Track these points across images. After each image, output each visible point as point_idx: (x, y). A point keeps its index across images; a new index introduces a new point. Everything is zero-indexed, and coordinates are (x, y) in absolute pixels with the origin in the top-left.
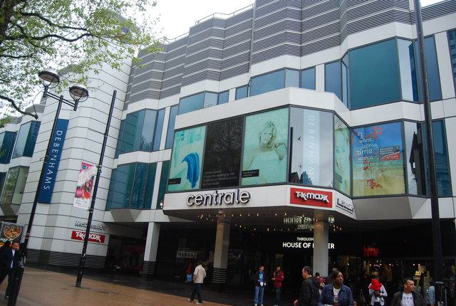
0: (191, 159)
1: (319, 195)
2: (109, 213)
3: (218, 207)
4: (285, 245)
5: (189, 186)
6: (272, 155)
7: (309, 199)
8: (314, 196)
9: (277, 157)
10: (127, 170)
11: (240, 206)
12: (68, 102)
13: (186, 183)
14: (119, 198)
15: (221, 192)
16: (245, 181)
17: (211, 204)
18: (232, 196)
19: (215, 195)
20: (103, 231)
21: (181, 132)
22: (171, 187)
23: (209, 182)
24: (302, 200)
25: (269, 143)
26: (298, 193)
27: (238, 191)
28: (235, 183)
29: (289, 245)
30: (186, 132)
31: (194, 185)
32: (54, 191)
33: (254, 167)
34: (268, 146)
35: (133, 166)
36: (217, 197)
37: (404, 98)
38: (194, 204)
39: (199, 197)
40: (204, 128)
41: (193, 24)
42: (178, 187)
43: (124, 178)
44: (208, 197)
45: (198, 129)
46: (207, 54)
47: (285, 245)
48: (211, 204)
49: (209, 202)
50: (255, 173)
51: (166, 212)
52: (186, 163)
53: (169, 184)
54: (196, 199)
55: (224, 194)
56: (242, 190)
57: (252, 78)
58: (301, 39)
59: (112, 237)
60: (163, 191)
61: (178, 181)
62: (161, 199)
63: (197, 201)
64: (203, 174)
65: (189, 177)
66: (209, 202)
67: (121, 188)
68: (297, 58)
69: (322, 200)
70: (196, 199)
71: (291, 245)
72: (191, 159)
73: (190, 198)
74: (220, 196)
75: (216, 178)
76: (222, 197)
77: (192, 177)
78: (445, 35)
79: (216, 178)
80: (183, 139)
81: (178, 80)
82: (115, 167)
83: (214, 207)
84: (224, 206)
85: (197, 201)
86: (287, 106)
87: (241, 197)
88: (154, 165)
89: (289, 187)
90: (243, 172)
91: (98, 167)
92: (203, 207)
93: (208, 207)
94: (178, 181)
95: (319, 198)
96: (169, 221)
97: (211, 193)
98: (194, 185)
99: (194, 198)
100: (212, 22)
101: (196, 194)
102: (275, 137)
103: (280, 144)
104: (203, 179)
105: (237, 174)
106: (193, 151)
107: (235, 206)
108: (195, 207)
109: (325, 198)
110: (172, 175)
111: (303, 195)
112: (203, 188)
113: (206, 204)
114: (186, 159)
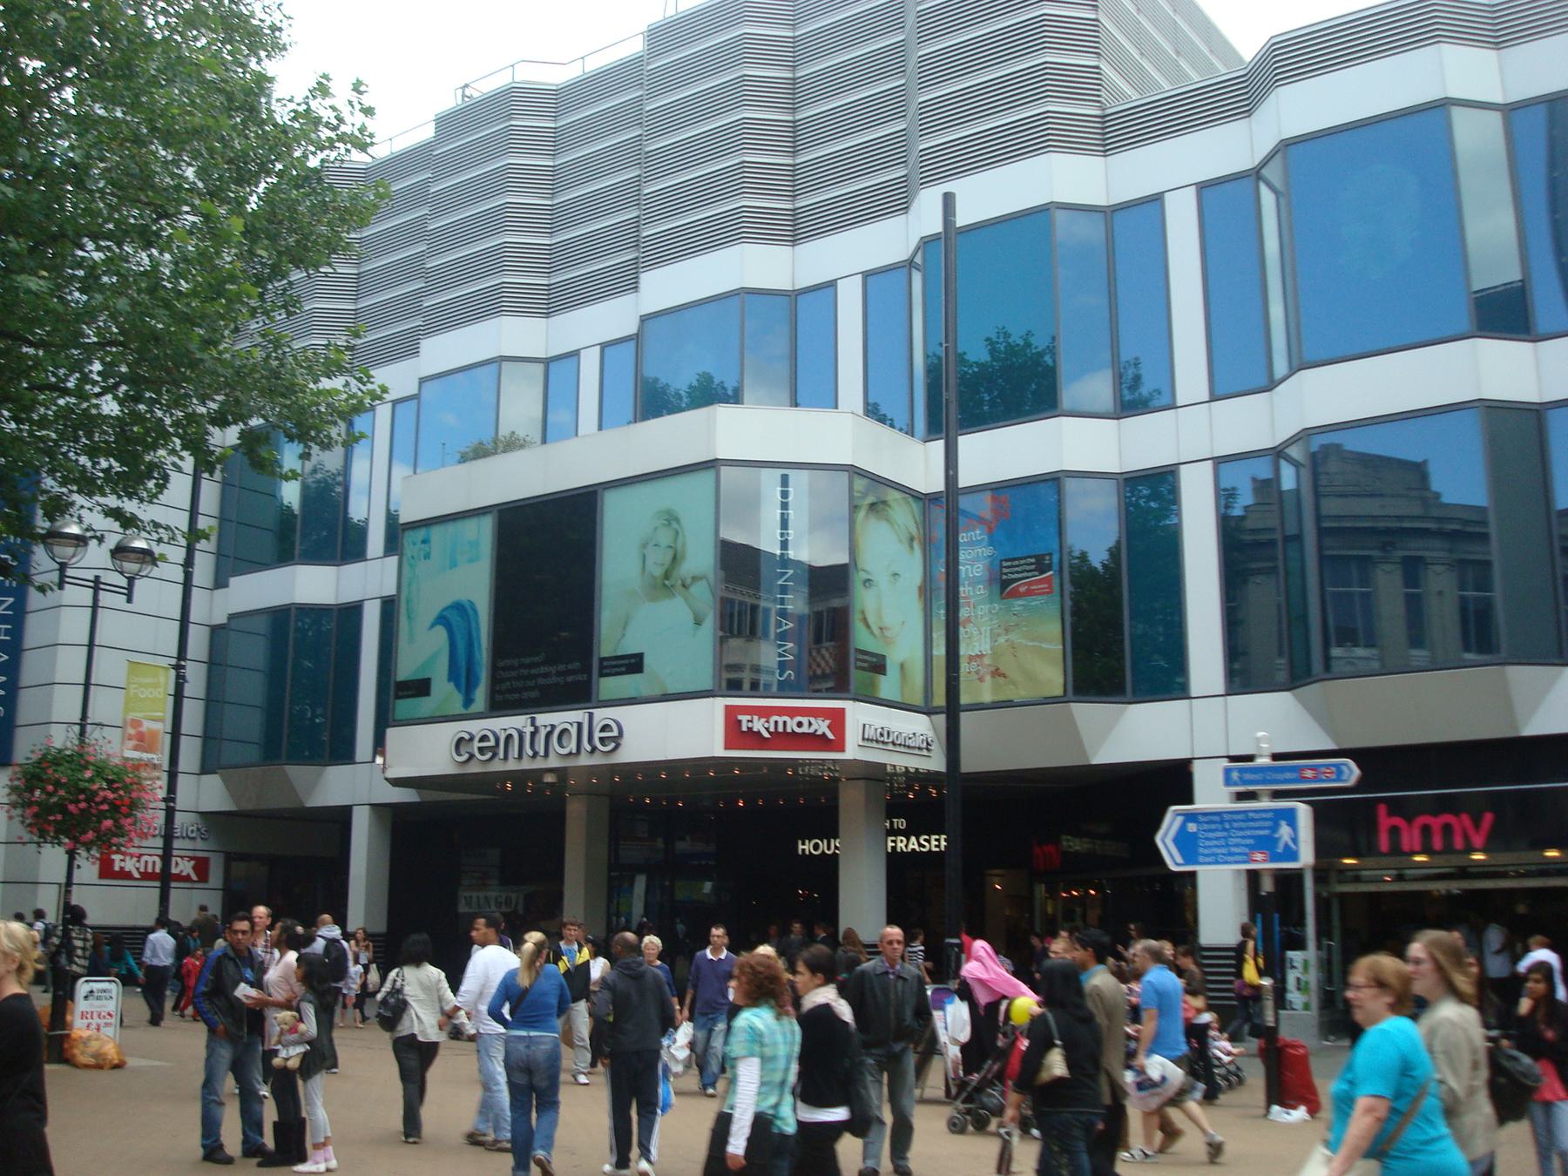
0: (454, 618)
1: (805, 720)
2: (213, 782)
3: (539, 764)
4: (806, 847)
5: (456, 704)
6: (675, 611)
7: (775, 734)
8: (792, 725)
9: (689, 617)
10: (262, 625)
11: (597, 760)
12: (113, 589)
13: (444, 692)
14: (248, 723)
15: (544, 719)
16: (609, 686)
17: (520, 756)
18: (574, 731)
19: (529, 729)
20: (200, 844)
21: (421, 534)
22: (404, 707)
23: (512, 691)
24: (754, 739)
25: (667, 576)
26: (744, 718)
27: (591, 715)
28: (579, 694)
29: (816, 847)
30: (436, 532)
31: (468, 701)
32: (21, 720)
33: (629, 648)
34: (666, 583)
35: (282, 618)
36: (533, 734)
37: (1495, 118)
38: (472, 756)
39: (484, 738)
40: (487, 526)
41: (449, 101)
42: (423, 706)
43: (252, 652)
44: (509, 737)
45: (470, 525)
46: (495, 221)
47: (806, 847)
48: (520, 756)
49: (514, 751)
50: (634, 664)
51: (397, 782)
52: (441, 632)
53: (398, 697)
54: (476, 744)
55: (553, 727)
56: (602, 715)
57: (644, 319)
58: (795, 180)
59: (229, 858)
60: (384, 721)
61: (421, 687)
62: (379, 745)
63: (481, 750)
64: (494, 669)
65: (453, 676)
66: (514, 751)
67: (250, 687)
68: (782, 252)
69: (813, 735)
70: (476, 744)
71: (823, 845)
72: (454, 618)
73: (461, 740)
74: (543, 732)
75: (530, 677)
76: (549, 735)
77: (463, 677)
78: (1190, 195)
79: (530, 677)
80: (427, 556)
81: (409, 306)
82: (221, 619)
83: (526, 765)
84: (553, 762)
85: (481, 750)
86: (712, 465)
87: (597, 735)
88: (352, 612)
89: (719, 705)
90: (602, 660)
91: (178, 667)
92: (498, 766)
93: (512, 765)
94: (421, 687)
95: (805, 729)
96: (418, 800)
97: (519, 722)
98: (468, 701)
99: (472, 739)
100: (508, 101)
101: (476, 727)
102: (683, 557)
103: (695, 579)
104: (495, 680)
105: (587, 669)
106: (461, 596)
107: (584, 760)
108: (474, 768)
109: (822, 727)
110: (405, 669)
111: (759, 725)
112: (500, 705)
113: (506, 758)
114: (442, 620)
